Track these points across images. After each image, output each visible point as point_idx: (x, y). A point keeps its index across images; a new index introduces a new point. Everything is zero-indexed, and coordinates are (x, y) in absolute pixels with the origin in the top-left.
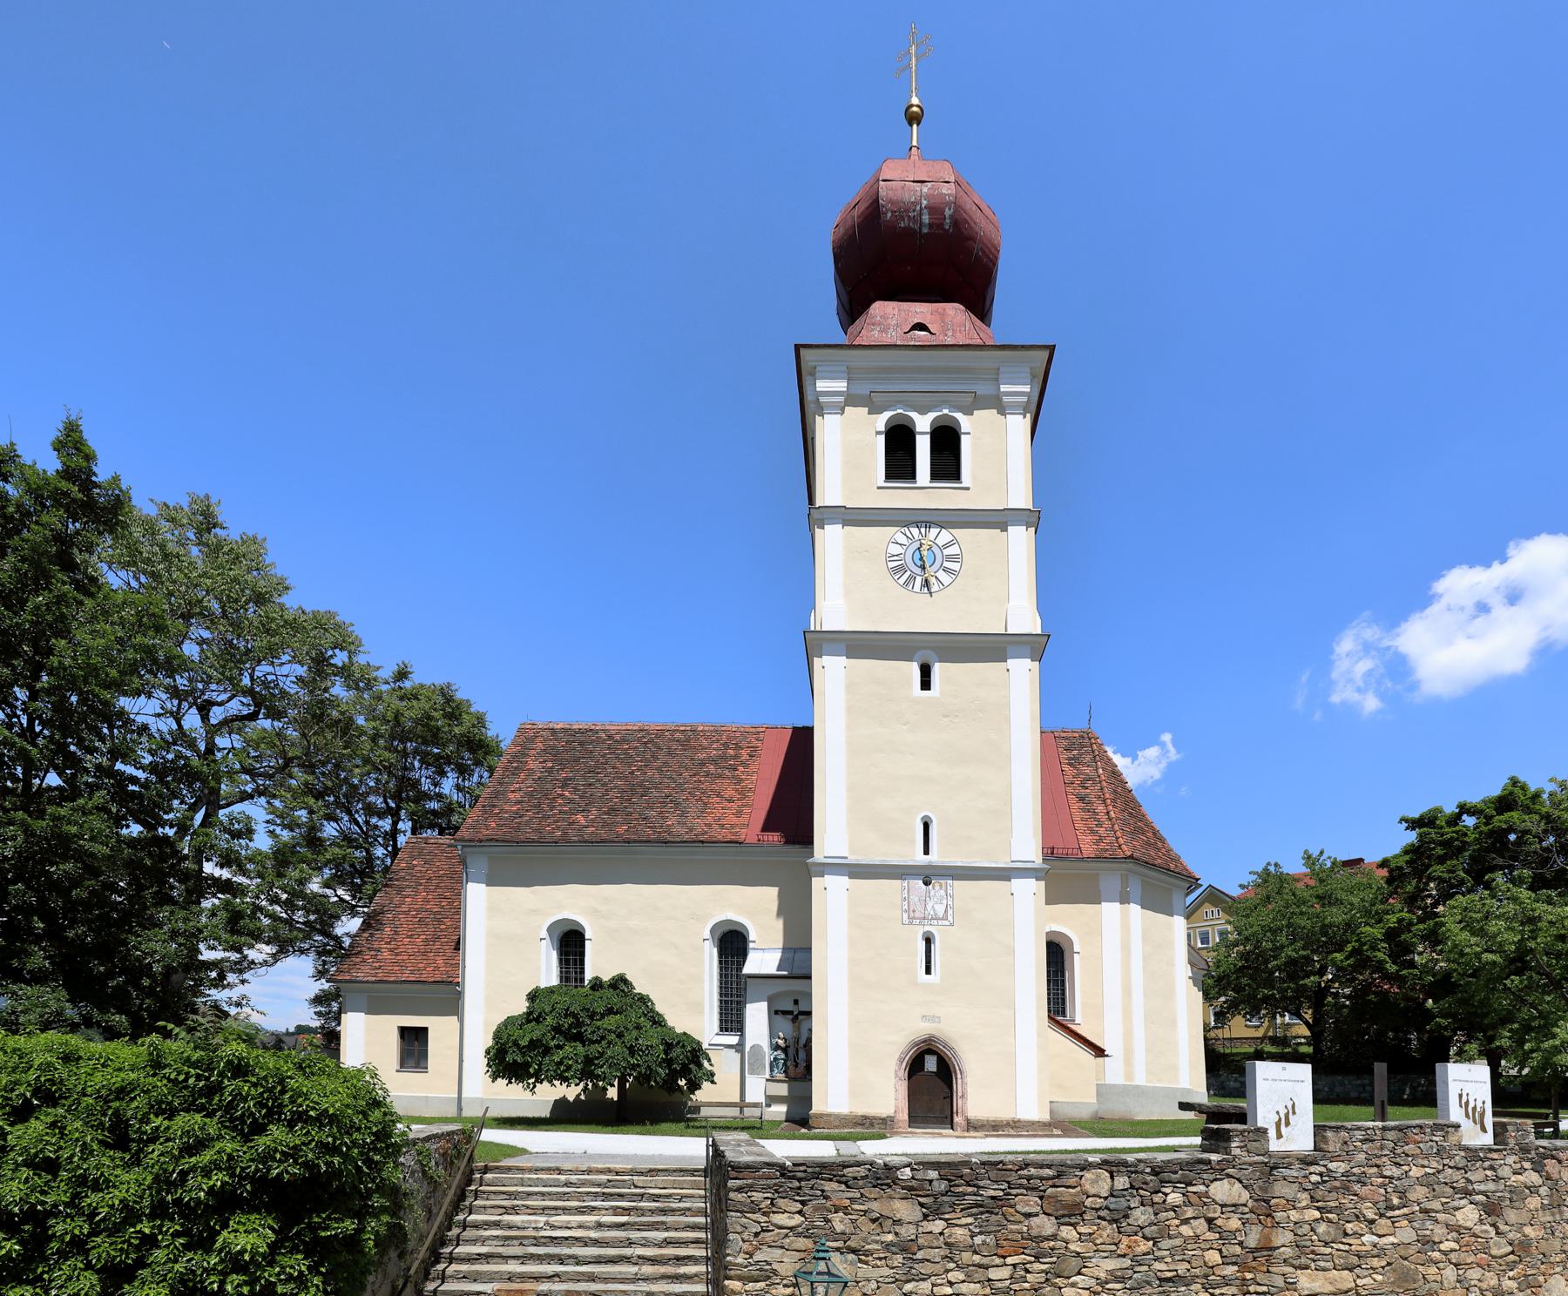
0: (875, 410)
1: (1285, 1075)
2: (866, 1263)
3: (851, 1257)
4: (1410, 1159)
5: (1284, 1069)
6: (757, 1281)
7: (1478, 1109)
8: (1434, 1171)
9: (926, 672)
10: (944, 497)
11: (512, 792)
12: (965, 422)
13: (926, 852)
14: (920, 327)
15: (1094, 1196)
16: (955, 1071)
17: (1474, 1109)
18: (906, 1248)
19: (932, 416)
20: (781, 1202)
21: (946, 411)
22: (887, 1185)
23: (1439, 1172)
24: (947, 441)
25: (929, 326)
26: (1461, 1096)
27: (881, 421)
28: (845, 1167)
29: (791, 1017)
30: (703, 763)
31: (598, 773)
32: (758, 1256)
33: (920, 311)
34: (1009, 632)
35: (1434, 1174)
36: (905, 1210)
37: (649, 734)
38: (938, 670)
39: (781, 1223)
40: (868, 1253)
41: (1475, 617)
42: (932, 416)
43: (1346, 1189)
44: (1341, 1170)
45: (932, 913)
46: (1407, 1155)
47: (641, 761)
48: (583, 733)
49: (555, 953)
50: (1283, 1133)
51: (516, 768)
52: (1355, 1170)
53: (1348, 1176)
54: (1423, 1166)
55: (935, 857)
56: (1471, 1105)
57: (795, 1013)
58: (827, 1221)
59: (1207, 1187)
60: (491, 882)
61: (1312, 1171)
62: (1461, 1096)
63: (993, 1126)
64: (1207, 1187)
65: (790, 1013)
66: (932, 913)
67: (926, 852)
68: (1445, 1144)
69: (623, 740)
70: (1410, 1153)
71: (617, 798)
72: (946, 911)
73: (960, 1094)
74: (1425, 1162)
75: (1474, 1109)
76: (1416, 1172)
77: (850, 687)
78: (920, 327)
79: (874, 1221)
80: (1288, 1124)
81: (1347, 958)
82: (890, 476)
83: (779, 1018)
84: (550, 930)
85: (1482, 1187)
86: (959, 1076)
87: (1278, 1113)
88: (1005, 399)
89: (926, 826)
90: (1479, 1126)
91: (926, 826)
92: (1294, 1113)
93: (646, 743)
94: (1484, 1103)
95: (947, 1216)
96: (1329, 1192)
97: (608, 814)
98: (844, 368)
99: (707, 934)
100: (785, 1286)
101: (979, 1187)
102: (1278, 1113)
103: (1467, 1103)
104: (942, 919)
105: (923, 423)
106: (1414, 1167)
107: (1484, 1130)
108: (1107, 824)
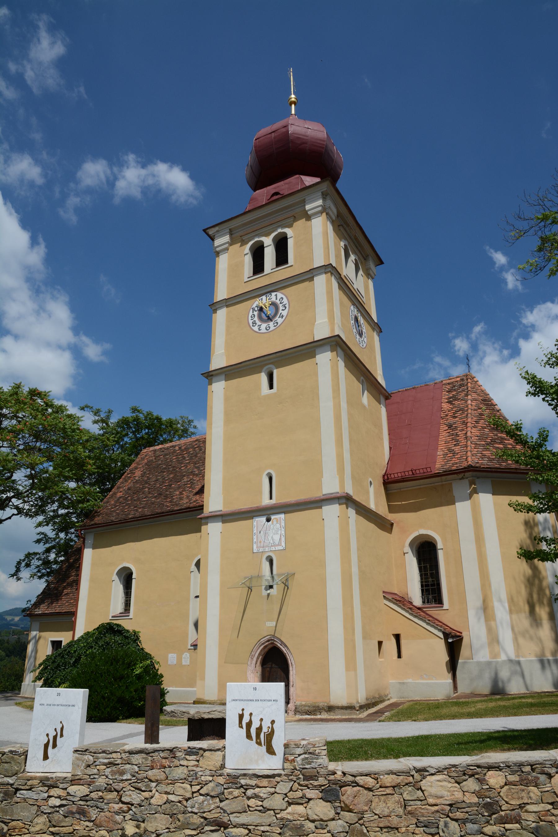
1: (59, 700)
4: (154, 784)
5: (59, 694)
7: (265, 729)
8: (180, 798)
10: (284, 273)
12: (289, 232)
13: (271, 498)
15: (362, 786)
17: (259, 730)
21: (280, 230)
23: (187, 800)
26: (241, 717)
27: (247, 248)
34: (315, 340)
35: (180, 802)
41: (60, 347)
43: (82, 813)
44: (79, 794)
45: (271, 542)
46: (151, 781)
49: (122, 586)
50: (49, 755)
52: (93, 795)
53: (87, 801)
54: (167, 793)
56: (255, 725)
59: (275, 788)
60: (94, 547)
61: (51, 794)
62: (241, 717)
64: (275, 788)
66: (271, 542)
68: (198, 769)
70: (153, 779)
74: (169, 788)
75: (259, 730)
76: (158, 799)
77: (227, 399)
80: (54, 746)
85: (243, 819)
87: (47, 735)
88: (309, 213)
90: (264, 748)
91: (271, 479)
92: (62, 735)
94: (273, 722)
96: (65, 817)
102: (47, 735)
103: (249, 725)
104: (278, 545)
106: (157, 793)
107: (270, 751)
108: (463, 442)
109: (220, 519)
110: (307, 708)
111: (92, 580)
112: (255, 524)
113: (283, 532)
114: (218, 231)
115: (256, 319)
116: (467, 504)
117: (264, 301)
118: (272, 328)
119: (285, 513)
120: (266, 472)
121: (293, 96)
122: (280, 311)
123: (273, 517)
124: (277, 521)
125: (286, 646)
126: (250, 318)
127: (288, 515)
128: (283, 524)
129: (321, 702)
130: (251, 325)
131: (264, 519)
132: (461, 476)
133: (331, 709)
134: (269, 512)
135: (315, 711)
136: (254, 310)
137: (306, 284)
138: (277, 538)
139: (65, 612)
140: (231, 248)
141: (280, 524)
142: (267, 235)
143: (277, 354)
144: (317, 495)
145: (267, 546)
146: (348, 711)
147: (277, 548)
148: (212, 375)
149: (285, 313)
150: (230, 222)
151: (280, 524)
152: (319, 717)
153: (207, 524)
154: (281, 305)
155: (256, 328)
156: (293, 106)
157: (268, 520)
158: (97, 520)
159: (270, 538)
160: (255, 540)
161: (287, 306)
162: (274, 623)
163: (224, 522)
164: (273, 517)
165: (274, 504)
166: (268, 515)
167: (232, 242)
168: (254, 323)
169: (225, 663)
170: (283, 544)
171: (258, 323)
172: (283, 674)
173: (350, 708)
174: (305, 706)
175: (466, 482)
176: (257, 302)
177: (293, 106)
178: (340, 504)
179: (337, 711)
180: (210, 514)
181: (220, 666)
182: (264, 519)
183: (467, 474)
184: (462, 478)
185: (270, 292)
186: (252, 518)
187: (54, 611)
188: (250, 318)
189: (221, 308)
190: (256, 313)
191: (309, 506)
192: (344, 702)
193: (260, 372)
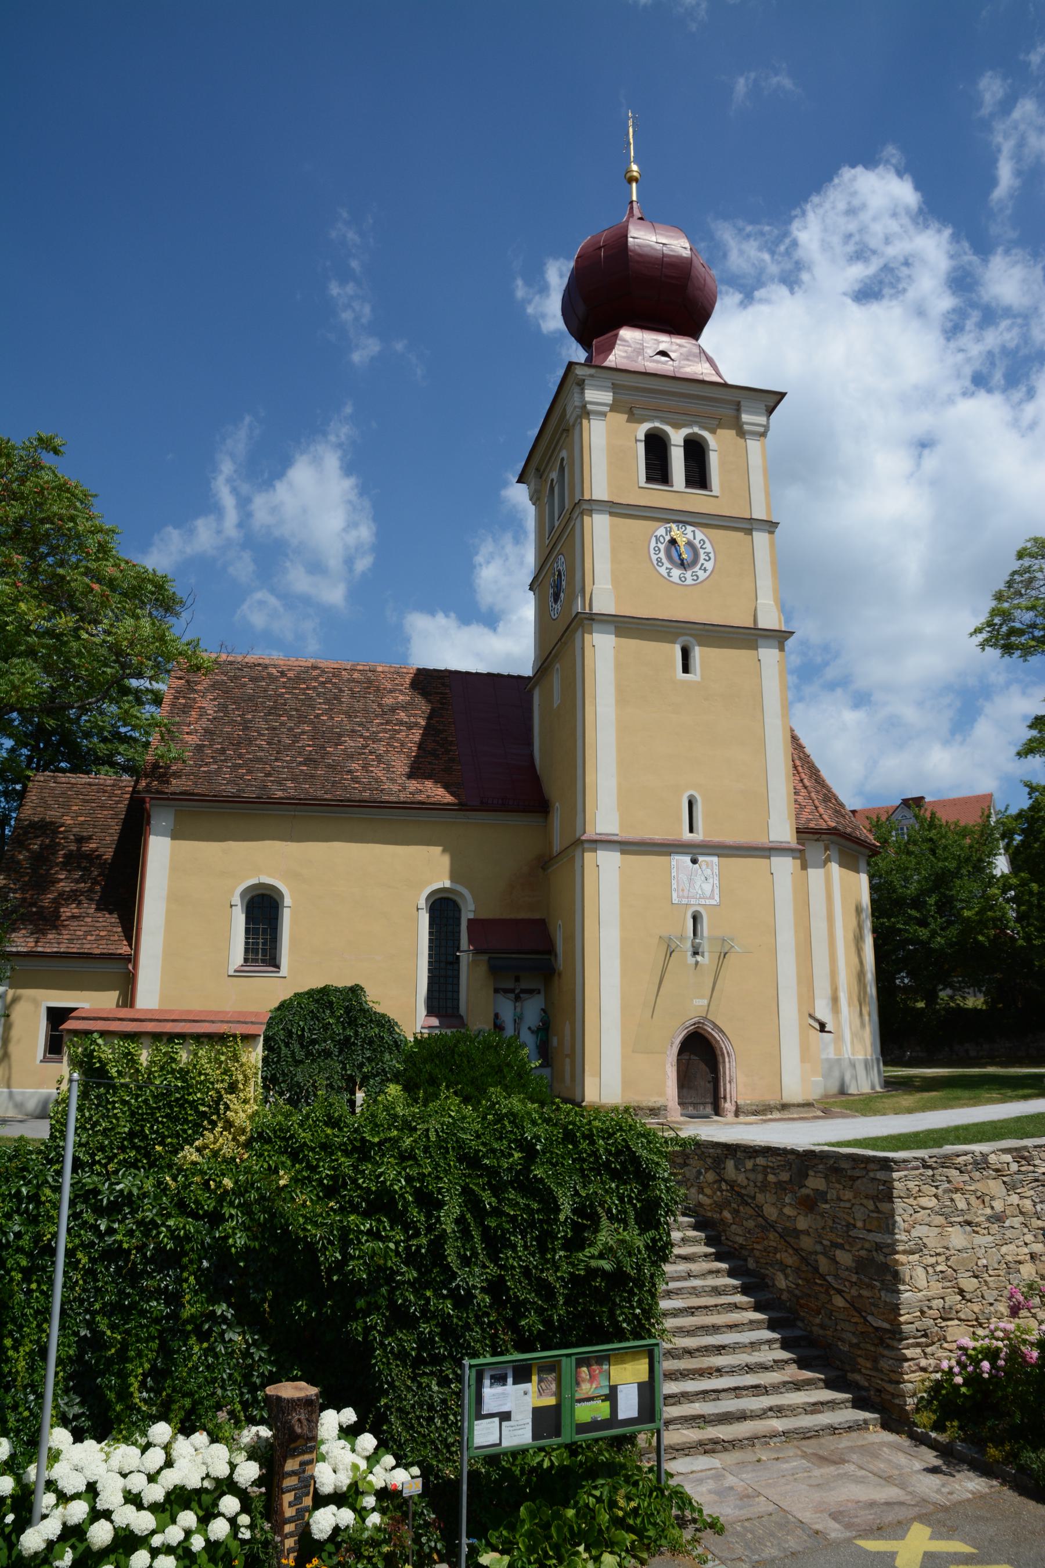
0: (634, 417)
2: (977, 1233)
3: (968, 1228)
6: (913, 1254)
9: (686, 654)
10: (696, 501)
11: (188, 733)
14: (663, 353)
16: (723, 1054)
18: (998, 1218)
19: (685, 431)
20: (924, 1188)
22: (984, 1168)
24: (696, 451)
25: (671, 354)
28: (958, 1156)
29: (512, 996)
30: (393, 710)
31: (280, 716)
32: (915, 1233)
33: (664, 341)
36: (995, 1187)
37: (323, 671)
38: (698, 653)
39: (925, 1205)
40: (978, 1225)
42: (685, 431)
47: (324, 703)
48: (250, 667)
51: (185, 705)
55: (698, 837)
57: (517, 991)
58: (952, 1200)
60: (175, 836)
63: (651, 1110)
65: (512, 991)
67: (691, 830)
69: (298, 679)
71: (309, 746)
72: (713, 891)
73: (728, 1078)
78: (663, 353)
79: (978, 1198)
81: (345, 742)
82: (649, 479)
83: (500, 997)
84: (243, 894)
86: (727, 1060)
89: (691, 805)
93: (323, 683)
95: (1018, 1191)
97: (305, 765)
98: (610, 385)
99: (422, 903)
100: (931, 1256)
101: (1035, 1166)
104: (710, 898)
105: (677, 437)
109: (618, 847)
110: (754, 1108)
111: (175, 898)
112: (674, 863)
113: (716, 882)
114: (592, 376)
115: (662, 555)
116: (821, 872)
117: (684, 535)
118: (689, 581)
119: (719, 856)
120: (692, 792)
121: (635, 167)
122: (702, 561)
123: (701, 859)
124: (707, 865)
125: (721, 1031)
126: (652, 551)
127: (724, 860)
128: (716, 871)
129: (772, 1099)
130: (655, 562)
131: (687, 859)
132: (816, 836)
133: (784, 1107)
134: (695, 851)
135: (765, 1110)
136: (657, 540)
137: (740, 535)
138: (707, 888)
139: (101, 954)
140: (609, 414)
141: (712, 870)
142: (677, 426)
143: (707, 627)
144: (760, 840)
145: (693, 898)
146: (806, 1109)
147: (708, 902)
148: (593, 620)
149: (709, 566)
150: (615, 373)
151: (712, 870)
152: (770, 1117)
153: (595, 850)
154: (702, 551)
155: (663, 571)
156: (634, 185)
157: (694, 861)
158: (176, 785)
159: (697, 887)
160: (674, 886)
161: (712, 555)
162: (705, 1002)
163: (623, 852)
164: (701, 859)
165: (703, 841)
166: (695, 854)
167: (614, 407)
168: (659, 560)
169: (633, 1052)
170: (717, 897)
171: (667, 564)
172: (703, 1067)
173: (808, 1105)
174: (751, 1105)
175: (821, 844)
176: (676, 532)
177: (634, 185)
178: (794, 858)
179: (793, 1109)
180: (598, 837)
181: (624, 1057)
182: (687, 859)
183: (824, 837)
184: (817, 840)
185: (686, 523)
186: (670, 854)
187: (55, 950)
188: (652, 551)
189: (600, 512)
190: (662, 547)
191: (752, 853)
192: (799, 1099)
193: (674, 642)
